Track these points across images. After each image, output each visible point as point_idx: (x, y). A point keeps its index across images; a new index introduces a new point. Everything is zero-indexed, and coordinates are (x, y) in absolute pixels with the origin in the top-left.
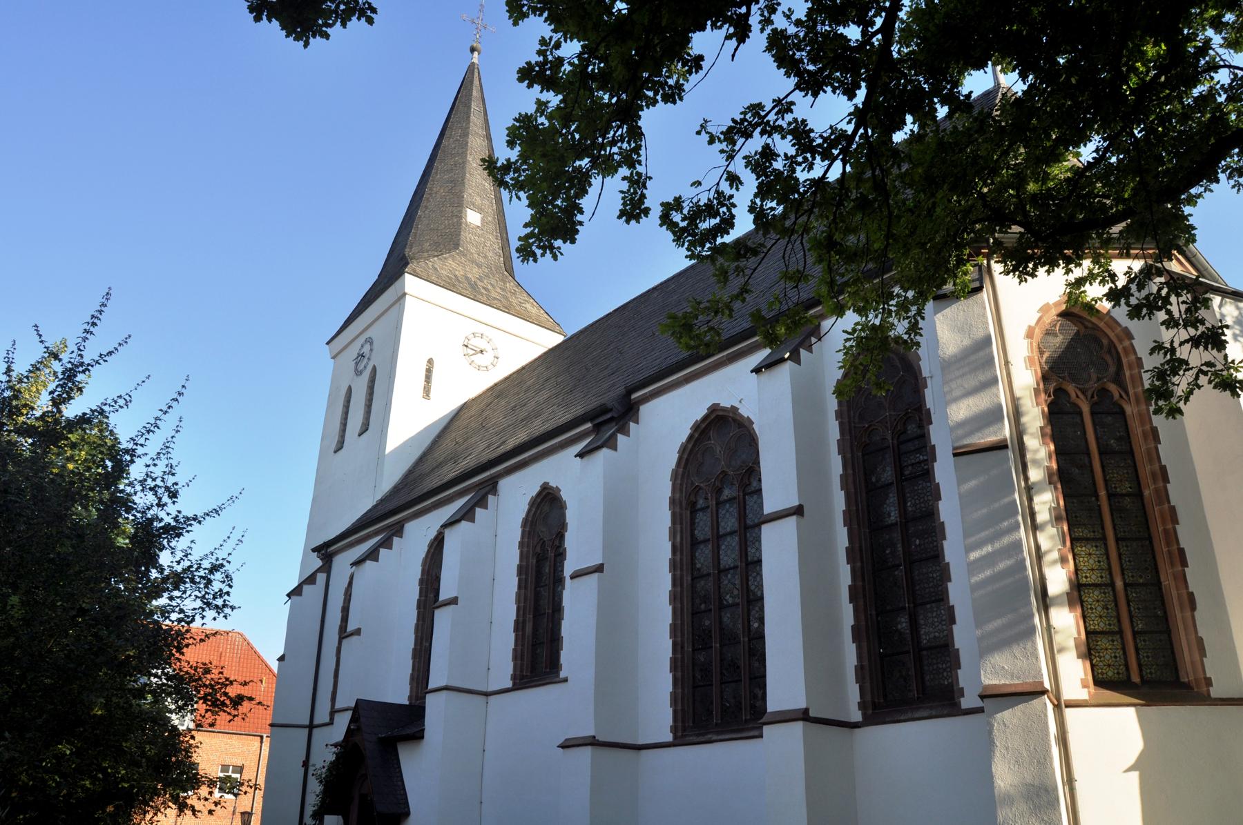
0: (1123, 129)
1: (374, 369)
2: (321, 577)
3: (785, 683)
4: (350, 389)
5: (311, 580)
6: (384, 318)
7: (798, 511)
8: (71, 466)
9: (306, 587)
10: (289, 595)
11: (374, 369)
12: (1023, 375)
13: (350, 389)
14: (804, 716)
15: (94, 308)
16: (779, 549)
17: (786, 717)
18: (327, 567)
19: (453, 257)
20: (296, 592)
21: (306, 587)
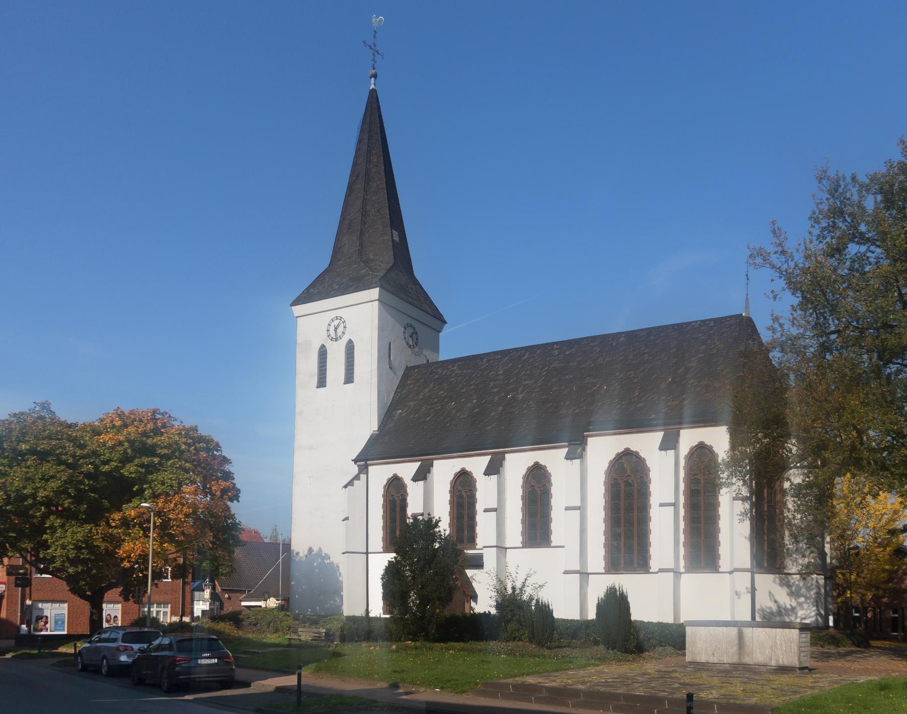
2: (362, 476)
5: (357, 477)
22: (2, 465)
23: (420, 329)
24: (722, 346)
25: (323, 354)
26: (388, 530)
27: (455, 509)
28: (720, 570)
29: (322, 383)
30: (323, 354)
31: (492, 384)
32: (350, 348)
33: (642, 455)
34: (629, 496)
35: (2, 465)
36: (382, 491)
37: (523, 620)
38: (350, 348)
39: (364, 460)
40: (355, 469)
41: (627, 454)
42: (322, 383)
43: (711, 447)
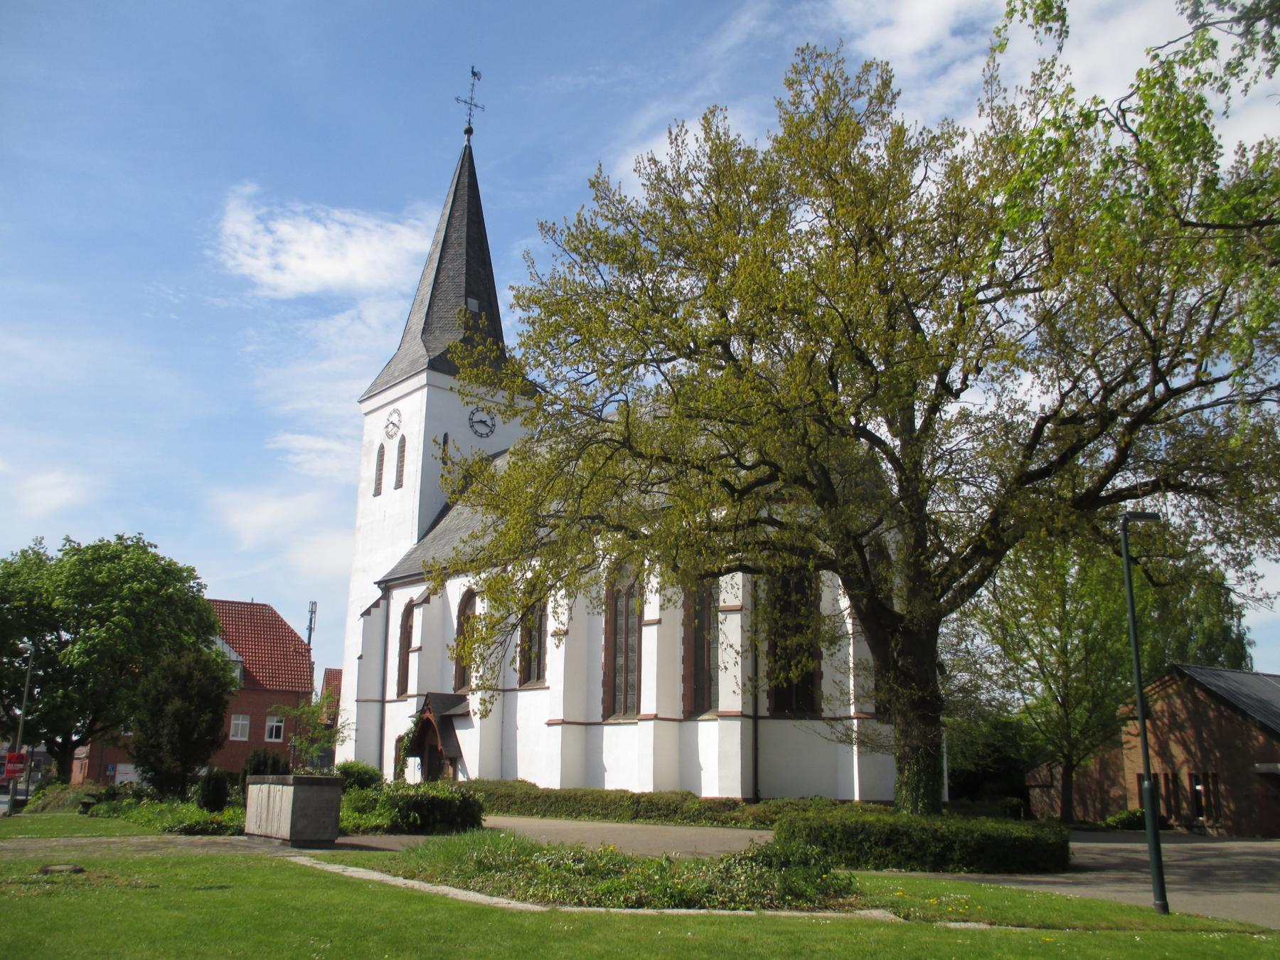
0: (1034, 654)
1: (403, 440)
2: (382, 603)
3: (649, 703)
4: (382, 447)
5: (376, 605)
6: (760, 740)
7: (659, 622)
8: (160, 627)
9: (373, 610)
10: (362, 615)
11: (403, 440)
12: (823, 650)
13: (382, 447)
14: (656, 717)
15: (308, 623)
16: (650, 636)
17: (647, 719)
18: (386, 596)
19: (918, 773)
20: (367, 613)
21: (373, 610)
28: (824, 715)
29: (378, 492)
42: (378, 492)
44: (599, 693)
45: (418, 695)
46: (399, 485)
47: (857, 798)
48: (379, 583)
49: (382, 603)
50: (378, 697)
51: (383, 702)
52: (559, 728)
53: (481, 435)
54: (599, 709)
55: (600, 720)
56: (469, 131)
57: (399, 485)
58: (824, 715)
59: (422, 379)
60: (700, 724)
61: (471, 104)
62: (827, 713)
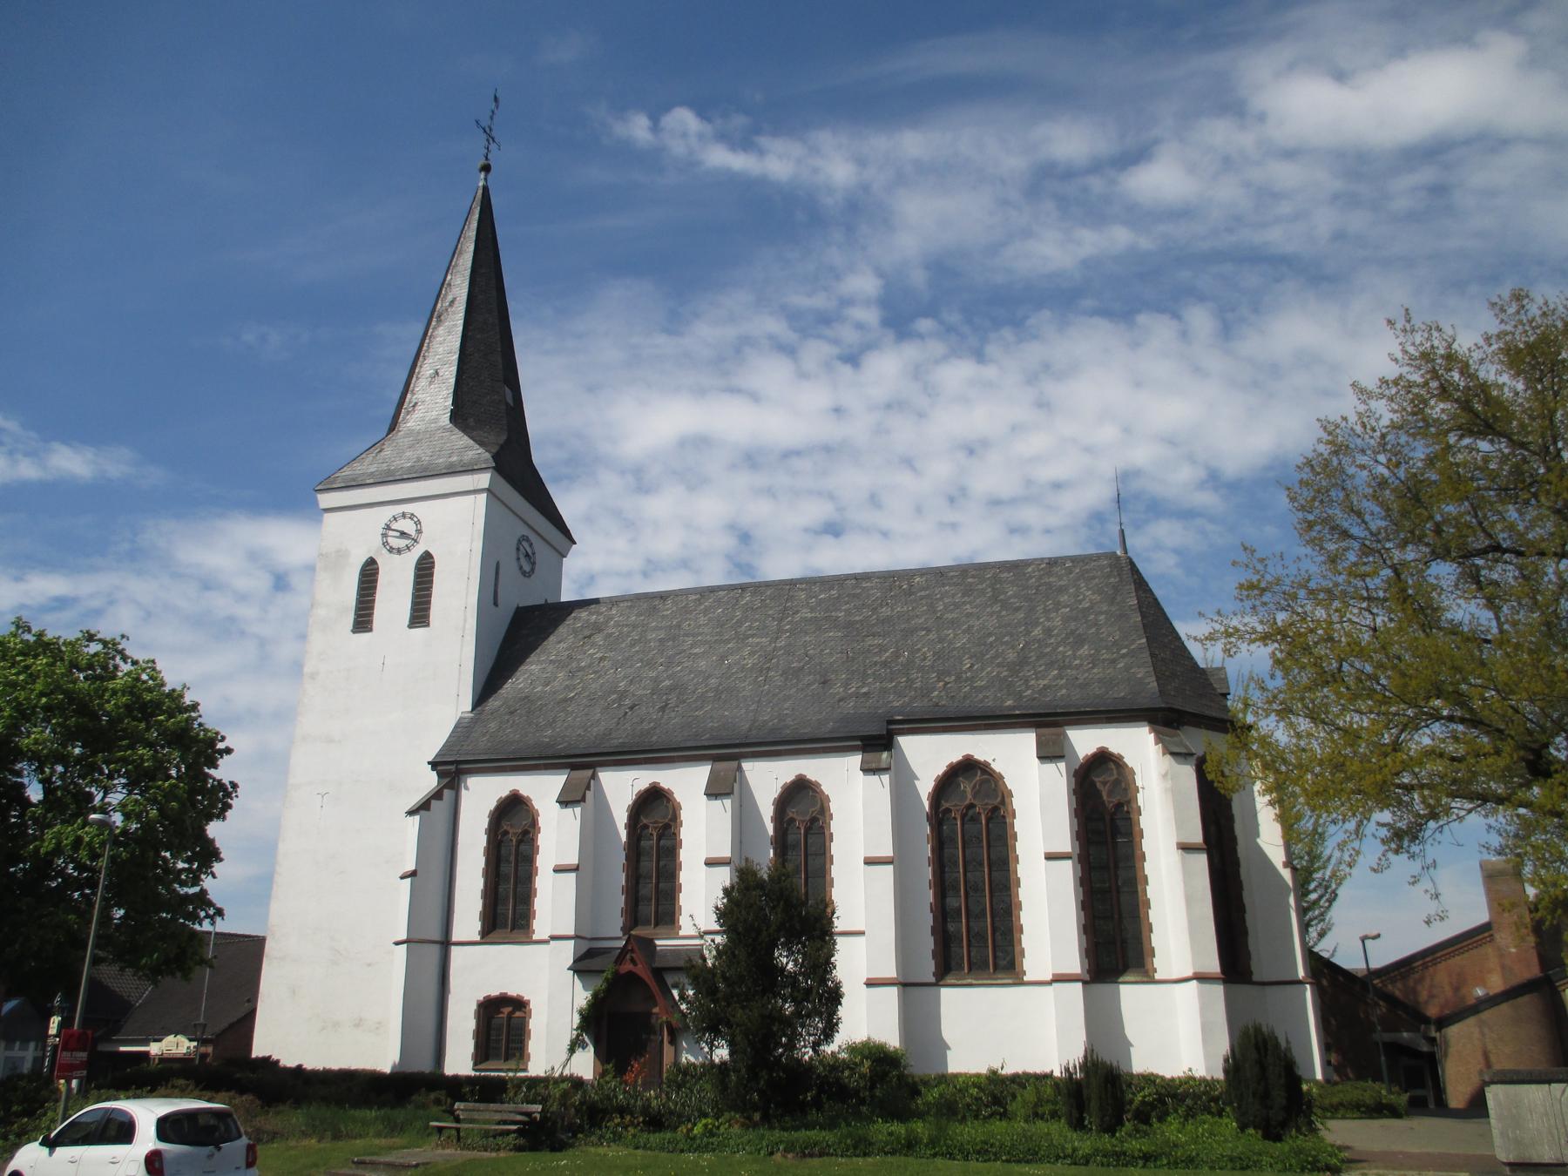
2: (446, 792)
5: (437, 795)
22: (4, 668)
23: (539, 546)
24: (1097, 597)
25: (369, 575)
26: (1017, 950)
27: (1140, 888)
28: (1157, 976)
29: (363, 622)
30: (369, 575)
31: (690, 641)
32: (425, 568)
33: (997, 767)
34: (513, 829)
35: (4, 668)
36: (484, 823)
37: (890, 1087)
38: (425, 568)
39: (452, 769)
40: (431, 780)
41: (968, 767)
42: (363, 622)
43: (1120, 758)
44: (929, 943)
45: (576, 937)
46: (420, 614)
47: (1319, 1076)
48: (434, 765)
49: (446, 792)
50: (436, 935)
51: (446, 943)
52: (1504, 1007)
53: (399, 551)
54: (930, 966)
55: (933, 980)
56: (486, 169)
57: (420, 614)
58: (1157, 976)
59: (484, 479)
60: (1123, 988)
61: (488, 133)
62: (1255, 978)
